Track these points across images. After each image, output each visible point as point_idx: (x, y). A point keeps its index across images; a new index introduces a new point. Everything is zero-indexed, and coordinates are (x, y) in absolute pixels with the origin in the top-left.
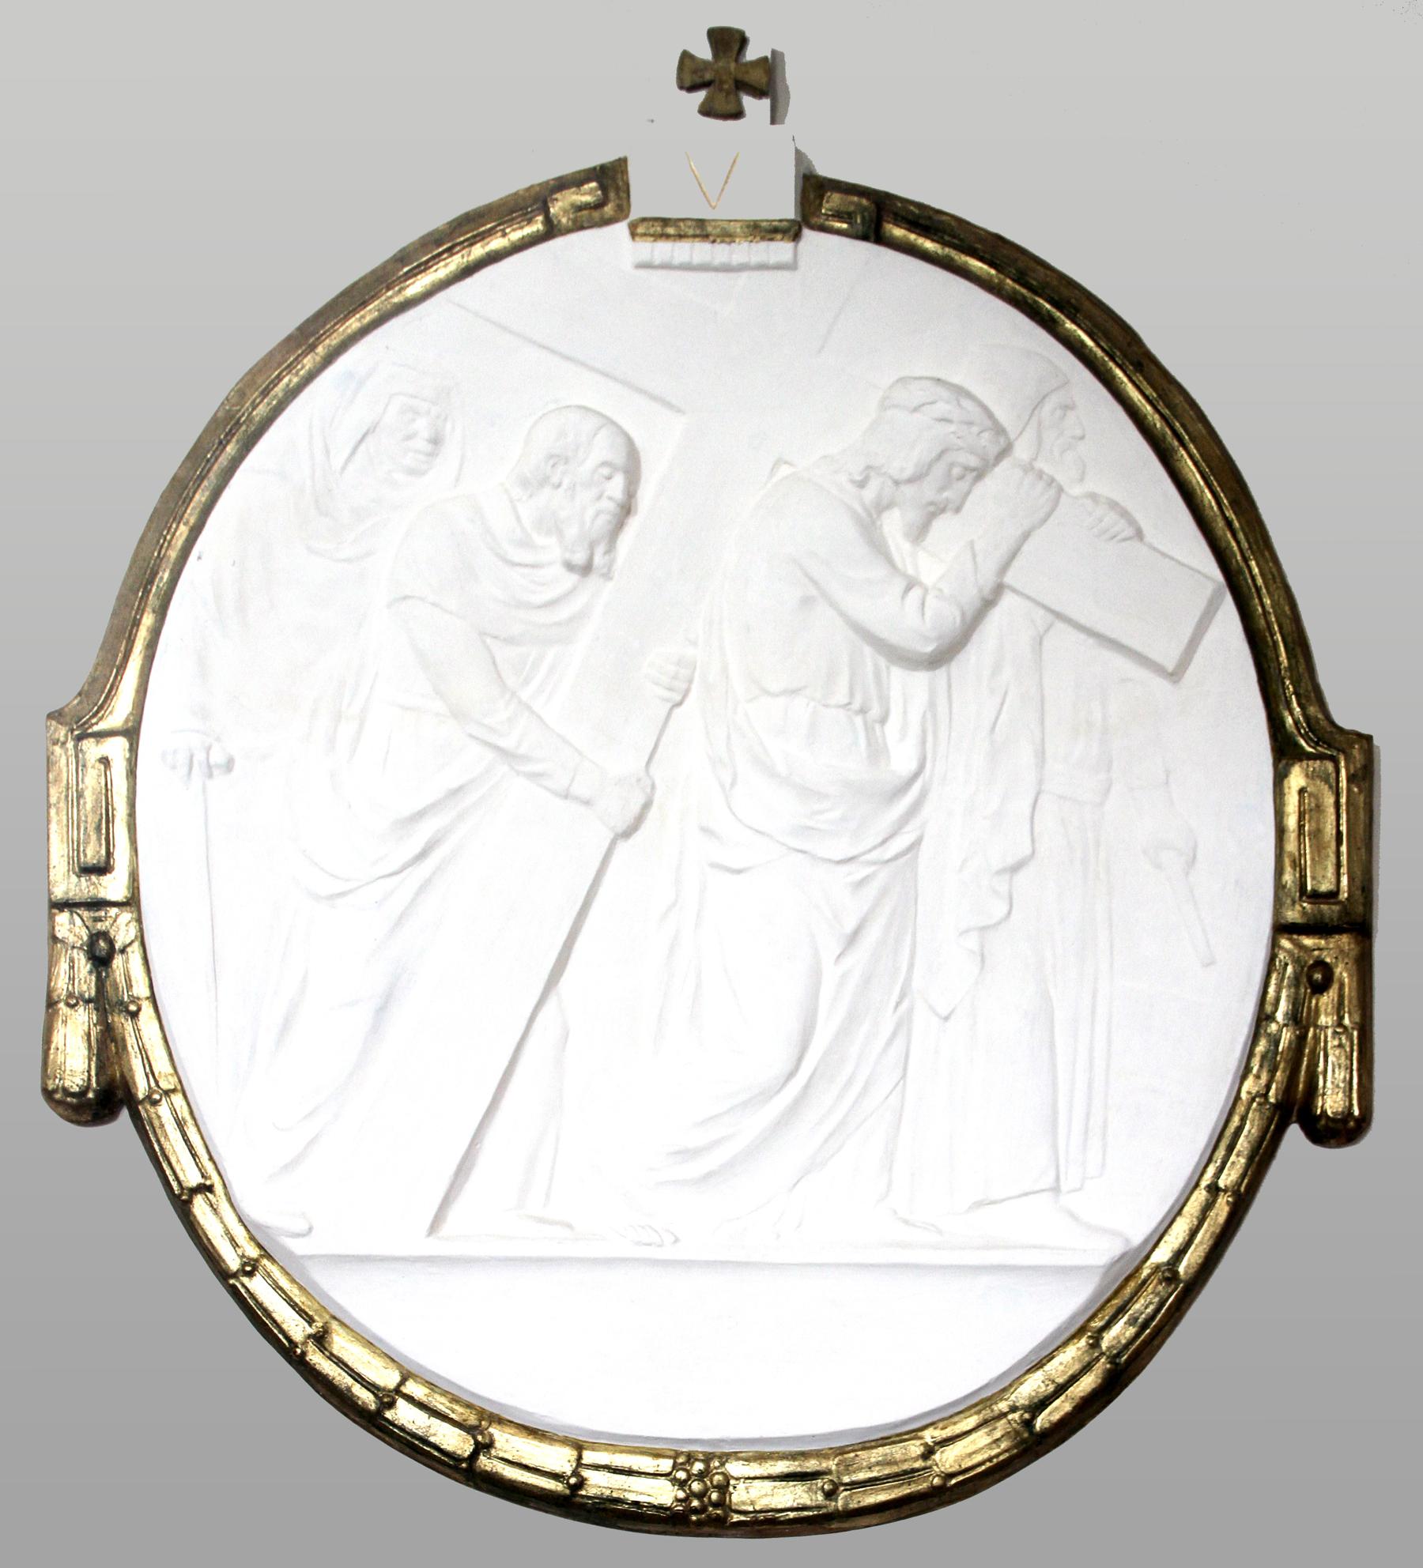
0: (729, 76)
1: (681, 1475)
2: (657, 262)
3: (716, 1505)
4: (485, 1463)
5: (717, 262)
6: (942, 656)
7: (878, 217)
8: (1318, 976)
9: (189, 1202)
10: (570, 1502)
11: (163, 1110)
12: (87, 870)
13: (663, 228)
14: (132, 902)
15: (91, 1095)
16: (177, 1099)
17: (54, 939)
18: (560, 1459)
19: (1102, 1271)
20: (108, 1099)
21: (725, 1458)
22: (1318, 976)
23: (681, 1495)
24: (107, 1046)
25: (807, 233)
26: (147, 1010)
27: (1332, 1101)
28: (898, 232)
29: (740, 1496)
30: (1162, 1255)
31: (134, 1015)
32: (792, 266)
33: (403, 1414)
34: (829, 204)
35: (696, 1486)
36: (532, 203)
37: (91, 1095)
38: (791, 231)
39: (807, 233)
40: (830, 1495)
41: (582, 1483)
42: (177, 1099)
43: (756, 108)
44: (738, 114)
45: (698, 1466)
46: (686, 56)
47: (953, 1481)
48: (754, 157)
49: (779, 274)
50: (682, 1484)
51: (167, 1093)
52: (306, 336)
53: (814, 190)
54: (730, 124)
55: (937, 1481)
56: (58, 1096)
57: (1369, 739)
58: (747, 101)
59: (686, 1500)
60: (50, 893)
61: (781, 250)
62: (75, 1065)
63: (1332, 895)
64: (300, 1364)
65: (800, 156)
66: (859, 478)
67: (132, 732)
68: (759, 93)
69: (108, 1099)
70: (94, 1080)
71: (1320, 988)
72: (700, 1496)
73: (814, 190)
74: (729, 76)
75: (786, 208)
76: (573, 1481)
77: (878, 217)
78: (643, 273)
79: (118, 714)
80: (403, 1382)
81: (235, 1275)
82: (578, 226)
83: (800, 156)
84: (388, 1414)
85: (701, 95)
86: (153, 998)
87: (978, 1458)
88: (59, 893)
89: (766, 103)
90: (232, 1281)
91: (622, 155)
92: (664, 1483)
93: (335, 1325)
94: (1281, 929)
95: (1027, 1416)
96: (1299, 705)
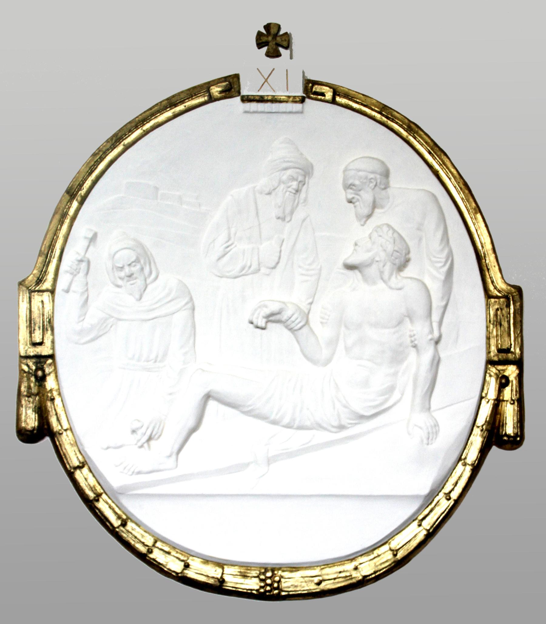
0: (273, 41)
1: (262, 577)
2: (251, 110)
5: (288, 110)
6: (274, 268)
9: (73, 473)
10: (218, 588)
12: (35, 344)
13: (246, 99)
16: (130, 525)
18: (215, 572)
22: (503, 381)
23: (262, 584)
24: (42, 413)
25: (307, 100)
27: (510, 429)
29: (284, 584)
30: (447, 489)
31: (53, 400)
32: (302, 112)
33: (157, 555)
34: (311, 90)
35: (269, 581)
37: (35, 432)
39: (307, 100)
44: (280, 55)
45: (269, 574)
48: (284, 75)
49: (298, 115)
50: (262, 580)
51: (66, 430)
52: (117, 139)
58: (281, 50)
60: (20, 353)
67: (52, 292)
68: (286, 48)
72: (270, 585)
75: (300, 93)
76: (221, 580)
78: (246, 115)
79: (47, 285)
80: (156, 542)
85: (265, 49)
87: (383, 566)
88: (23, 354)
89: (288, 51)
91: (237, 73)
92: (257, 580)
94: (490, 362)
95: (395, 553)
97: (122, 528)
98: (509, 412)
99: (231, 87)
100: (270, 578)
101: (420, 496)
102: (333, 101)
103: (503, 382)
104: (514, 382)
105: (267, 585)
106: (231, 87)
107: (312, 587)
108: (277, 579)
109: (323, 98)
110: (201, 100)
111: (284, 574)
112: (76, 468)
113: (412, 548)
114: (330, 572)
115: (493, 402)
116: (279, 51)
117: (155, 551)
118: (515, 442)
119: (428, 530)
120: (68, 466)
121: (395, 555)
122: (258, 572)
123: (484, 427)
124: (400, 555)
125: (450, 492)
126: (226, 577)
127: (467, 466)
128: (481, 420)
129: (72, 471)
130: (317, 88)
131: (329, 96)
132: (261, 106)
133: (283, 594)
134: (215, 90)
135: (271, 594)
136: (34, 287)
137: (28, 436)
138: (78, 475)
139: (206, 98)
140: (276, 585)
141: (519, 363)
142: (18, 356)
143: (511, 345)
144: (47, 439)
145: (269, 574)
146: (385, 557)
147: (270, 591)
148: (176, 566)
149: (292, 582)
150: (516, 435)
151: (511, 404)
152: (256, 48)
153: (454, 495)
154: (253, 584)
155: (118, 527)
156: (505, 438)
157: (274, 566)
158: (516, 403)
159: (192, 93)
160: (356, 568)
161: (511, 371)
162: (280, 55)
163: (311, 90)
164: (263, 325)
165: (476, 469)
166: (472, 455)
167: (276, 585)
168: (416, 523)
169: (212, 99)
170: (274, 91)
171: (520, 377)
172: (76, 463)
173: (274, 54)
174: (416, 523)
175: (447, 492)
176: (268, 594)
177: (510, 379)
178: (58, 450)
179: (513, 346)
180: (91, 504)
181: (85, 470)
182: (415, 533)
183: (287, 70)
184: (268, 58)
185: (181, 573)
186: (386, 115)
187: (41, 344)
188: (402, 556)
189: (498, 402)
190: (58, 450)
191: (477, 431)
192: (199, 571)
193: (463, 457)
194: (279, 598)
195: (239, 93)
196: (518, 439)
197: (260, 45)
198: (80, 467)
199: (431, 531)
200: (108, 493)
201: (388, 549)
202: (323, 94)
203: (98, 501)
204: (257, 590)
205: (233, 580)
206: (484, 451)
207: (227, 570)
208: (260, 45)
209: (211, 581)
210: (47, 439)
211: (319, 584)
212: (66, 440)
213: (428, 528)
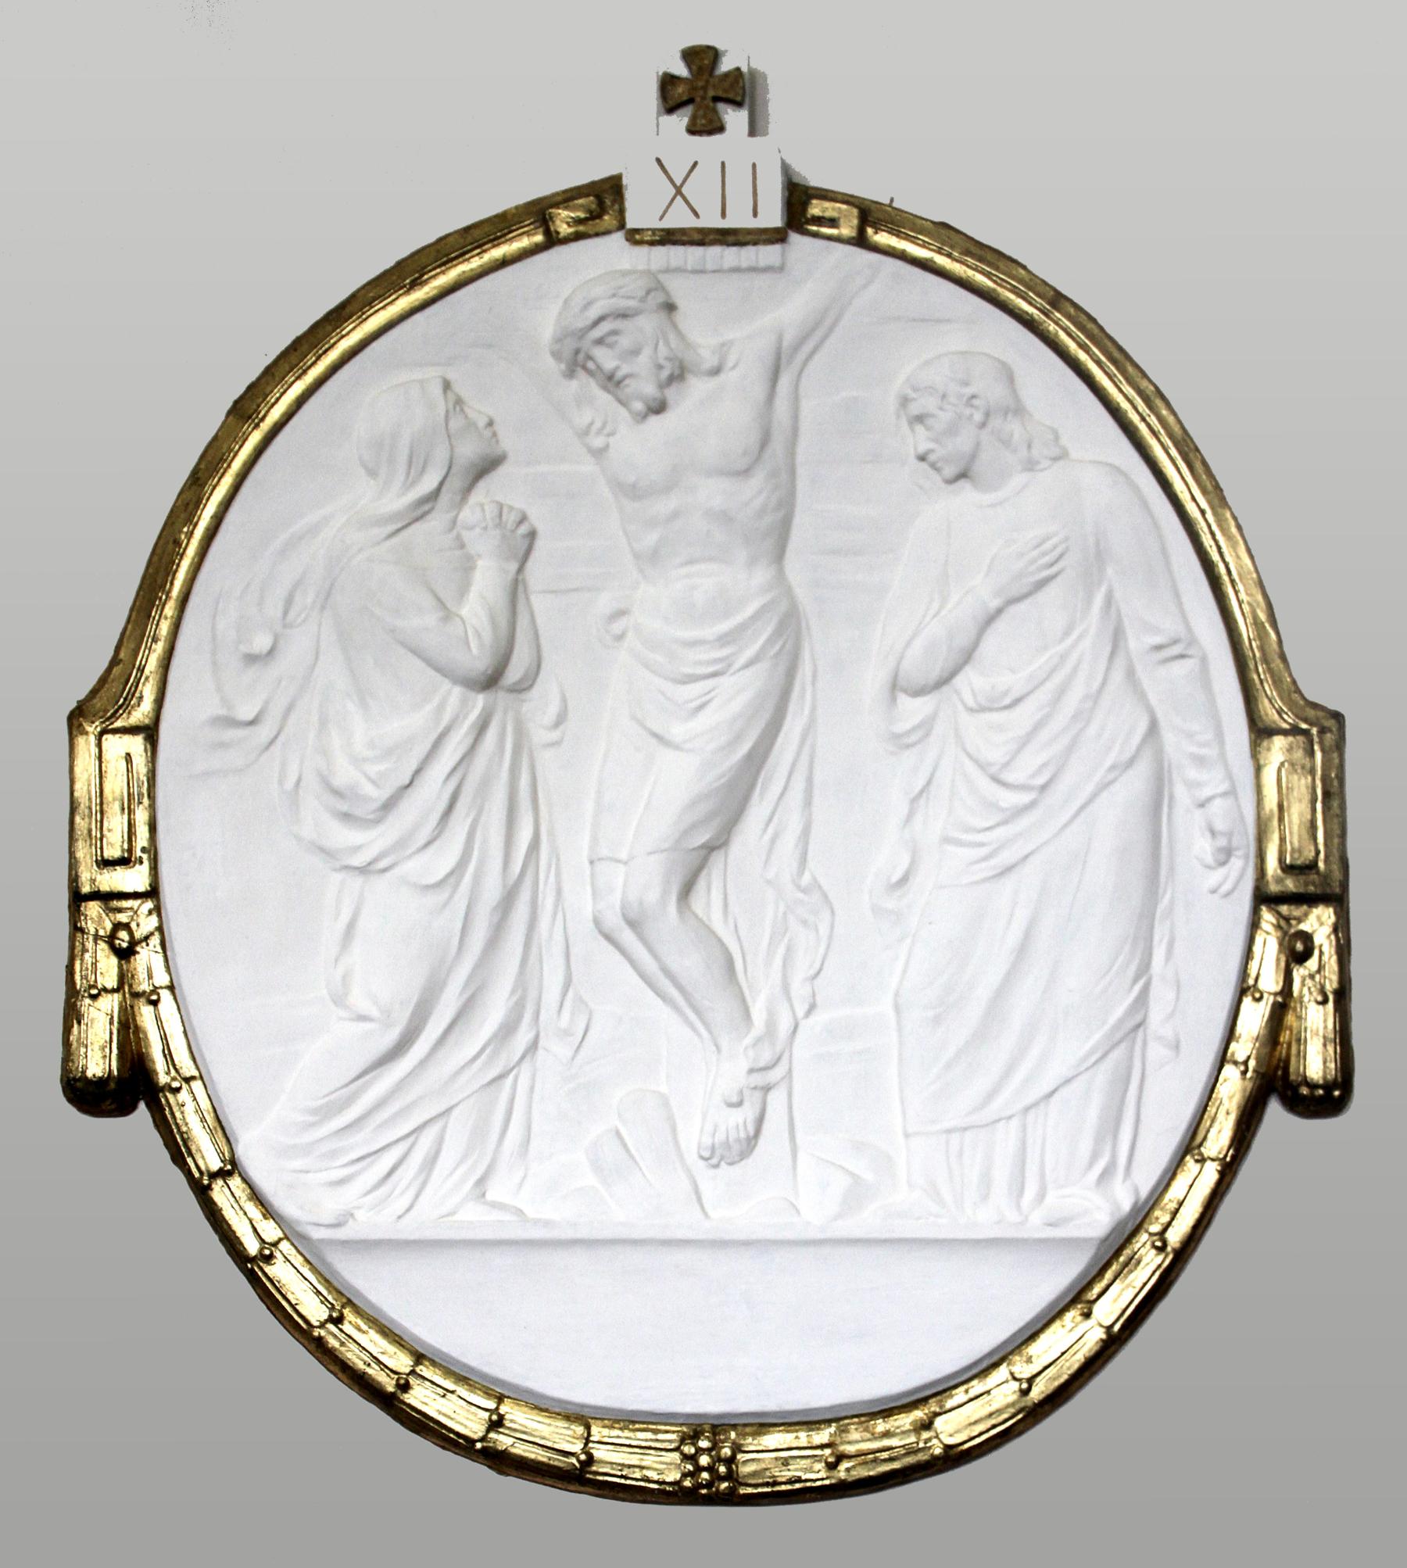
0: (705, 90)
1: (689, 1449)
4: (502, 1441)
8: (1299, 946)
9: (209, 1187)
10: (578, 1476)
11: (184, 1096)
13: (635, 237)
14: (153, 893)
15: (112, 1085)
16: (197, 1085)
18: (565, 1438)
19: (1096, 1243)
22: (1299, 946)
23: (690, 1467)
26: (165, 995)
27: (1316, 1063)
31: (155, 1003)
33: (420, 1397)
36: (539, 213)
38: (776, 237)
39: (794, 238)
40: (832, 1466)
41: (591, 1459)
42: (197, 1085)
43: (735, 119)
44: (721, 129)
48: (734, 169)
50: (686, 1458)
51: (188, 1080)
54: (716, 138)
55: (938, 1451)
57: (1338, 717)
61: (768, 254)
62: (98, 1062)
63: (1312, 866)
64: (320, 1349)
65: (786, 169)
68: (738, 104)
69: (129, 1088)
71: (1302, 958)
73: (800, 205)
75: (772, 216)
76: (583, 1457)
81: (253, 1260)
82: (578, 237)
83: (786, 169)
91: (614, 172)
94: (1263, 898)
98: (1316, 1020)
100: (708, 1450)
101: (1086, 1240)
102: (861, 241)
103: (1298, 950)
104: (1325, 949)
105: (699, 1469)
106: (603, 201)
107: (817, 1474)
108: (726, 1452)
109: (833, 231)
110: (524, 242)
112: (213, 1176)
113: (1076, 1366)
114: (856, 1441)
115: (1272, 998)
116: (727, 75)
118: (1327, 1100)
119: (1109, 1328)
121: (1025, 1393)
123: (1252, 1064)
124: (1037, 1393)
125: (1165, 1230)
126: (599, 1453)
127: (1209, 1163)
128: (1244, 1048)
129: (206, 1182)
130: (816, 209)
131: (847, 230)
132: (714, 254)
133: (742, 1491)
134: (563, 220)
136: (97, 708)
137: (90, 1096)
138: (219, 1194)
139: (539, 238)
141: (1338, 899)
143: (1318, 852)
145: (704, 1444)
146: (1000, 1393)
147: (709, 1485)
148: (469, 1422)
149: (764, 1456)
150: (1328, 1087)
151: (1319, 1003)
153: (1175, 1237)
154: (665, 1468)
155: (322, 1325)
157: (716, 1422)
158: (1330, 1005)
159: (499, 227)
161: (1319, 922)
162: (721, 129)
163: (800, 205)
164: (777, 264)
165: (1229, 1170)
166: (1219, 1139)
169: (552, 240)
170: (696, 214)
171: (1342, 927)
172: (215, 1164)
173: (707, 126)
176: (704, 1491)
177: (1317, 941)
179: (1322, 856)
180: (578, 1476)
181: (235, 1182)
182: (1072, 1340)
184: (696, 139)
185: (483, 1439)
186: (990, 273)
187: (124, 861)
188: (1042, 1397)
189: (1283, 1007)
191: (1230, 1072)
192: (534, 1433)
194: (731, 1499)
195: (622, 225)
196: (1337, 1093)
197: (670, 106)
198: (223, 1174)
199: (1117, 1328)
202: (833, 222)
203: (269, 1259)
205: (612, 1456)
208: (670, 106)
209: (559, 1461)
211: (832, 1466)
212: (189, 1110)
213: (1108, 1323)
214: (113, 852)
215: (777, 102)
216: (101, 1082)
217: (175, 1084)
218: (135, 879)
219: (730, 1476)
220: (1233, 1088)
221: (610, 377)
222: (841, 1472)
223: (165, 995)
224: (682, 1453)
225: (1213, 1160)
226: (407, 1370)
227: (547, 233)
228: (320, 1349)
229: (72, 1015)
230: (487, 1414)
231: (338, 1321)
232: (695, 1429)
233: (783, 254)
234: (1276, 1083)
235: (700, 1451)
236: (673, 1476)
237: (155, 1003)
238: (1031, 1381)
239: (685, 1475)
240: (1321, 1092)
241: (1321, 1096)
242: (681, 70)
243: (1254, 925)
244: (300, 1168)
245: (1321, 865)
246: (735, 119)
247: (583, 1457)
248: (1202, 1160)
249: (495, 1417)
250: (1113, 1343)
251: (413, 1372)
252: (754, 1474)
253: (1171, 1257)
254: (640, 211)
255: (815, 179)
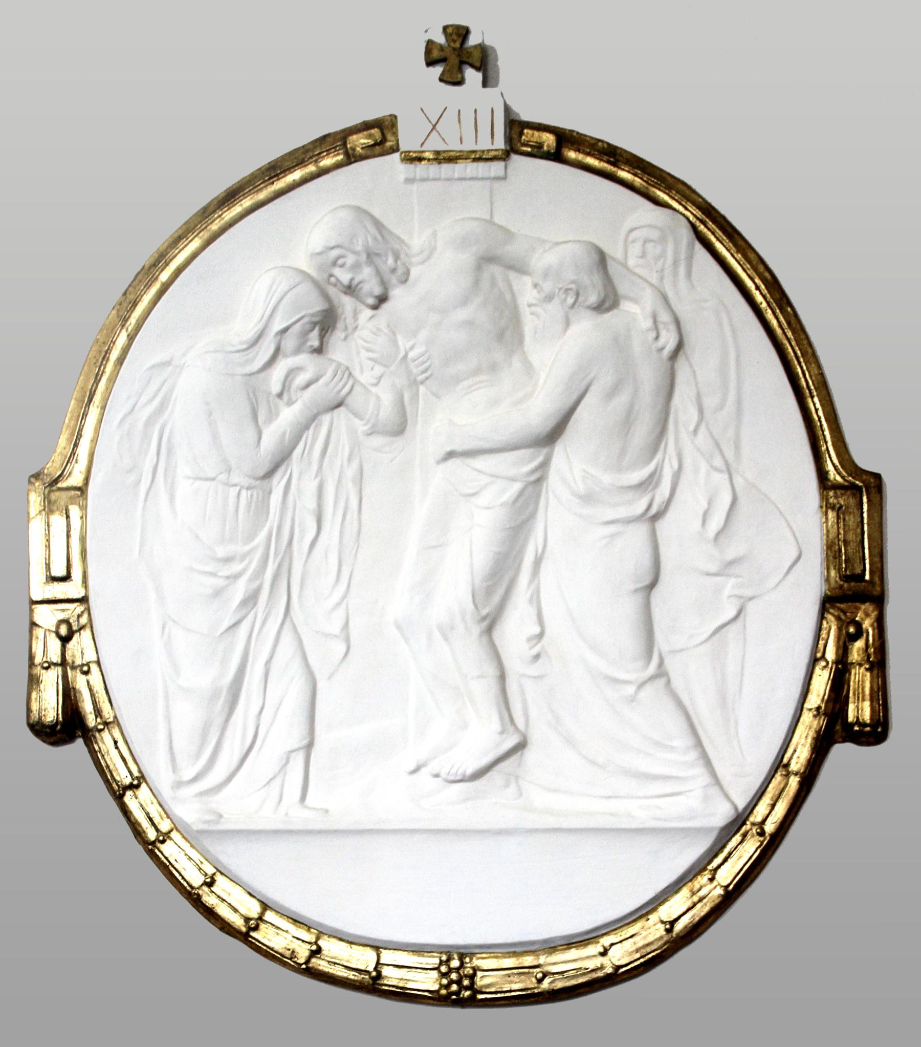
0: (458, 55)
3: (467, 988)
4: (320, 964)
7: (564, 146)
10: (372, 985)
16: (222, 883)
17: (33, 624)
18: (365, 959)
20: (70, 727)
21: (471, 955)
23: (445, 981)
26: (94, 667)
27: (860, 710)
28: (572, 155)
34: (518, 136)
35: (454, 976)
36: (337, 141)
38: (505, 156)
39: (514, 157)
41: (379, 976)
44: (459, 83)
45: (455, 963)
46: (430, 44)
47: (622, 970)
48: (472, 112)
53: (515, 127)
56: (37, 728)
57: (878, 477)
59: (447, 987)
61: (497, 168)
62: (49, 706)
64: (196, 901)
65: (507, 109)
66: (640, 254)
70: (60, 716)
73: (515, 127)
74: (458, 55)
75: (500, 143)
76: (374, 974)
77: (564, 146)
83: (507, 109)
84: (253, 934)
86: (98, 663)
90: (150, 847)
93: (218, 874)
95: (668, 926)
96: (844, 529)
97: (205, 888)
99: (381, 136)
100: (457, 970)
105: (451, 982)
106: (381, 136)
111: (476, 962)
117: (385, 971)
118: (875, 733)
120: (114, 785)
122: (437, 961)
128: (815, 699)
133: (480, 997)
135: (460, 991)
138: (128, 798)
139: (340, 157)
140: (466, 982)
142: (28, 601)
144: (80, 742)
145: (455, 963)
146: (651, 932)
147: (457, 993)
152: (424, 63)
153: (770, 828)
154: (428, 982)
156: (856, 728)
160: (604, 953)
163: (518, 136)
167: (466, 982)
168: (707, 875)
169: (351, 158)
172: (127, 781)
173: (453, 79)
174: (707, 875)
175: (759, 819)
176: (454, 997)
178: (93, 753)
183: (476, 110)
187: (66, 578)
190: (93, 753)
192: (341, 957)
193: (785, 761)
194: (472, 1002)
198: (131, 787)
199: (731, 887)
200: (179, 827)
201: (658, 920)
204: (438, 991)
206: (821, 747)
207: (387, 956)
210: (80, 742)
213: (725, 884)
214: (60, 571)
215: (504, 64)
216: (53, 726)
217: (101, 727)
218: (73, 589)
219: (471, 987)
220: (809, 726)
221: (349, 287)
222: (545, 985)
223: (94, 667)
224: (440, 972)
225: (796, 774)
226: (256, 916)
227: (347, 154)
228: (196, 901)
229: (34, 681)
230: (308, 946)
231: (210, 884)
232: (448, 952)
233: (506, 168)
234: (835, 728)
235: (450, 970)
236: (435, 987)
237: (86, 673)
238: (673, 923)
239: (442, 986)
240: (868, 729)
241: (869, 732)
242: (441, 39)
243: (822, 617)
244: (173, 795)
245: (867, 577)
246: (472, 76)
247: (374, 974)
248: (787, 775)
249: (314, 948)
250: (731, 896)
251: (260, 918)
252: (488, 986)
253: (768, 838)
254: (409, 137)
255: (525, 117)
